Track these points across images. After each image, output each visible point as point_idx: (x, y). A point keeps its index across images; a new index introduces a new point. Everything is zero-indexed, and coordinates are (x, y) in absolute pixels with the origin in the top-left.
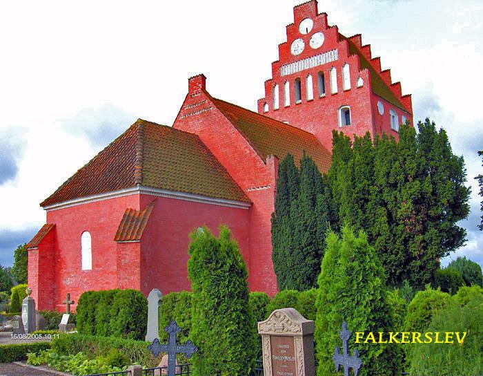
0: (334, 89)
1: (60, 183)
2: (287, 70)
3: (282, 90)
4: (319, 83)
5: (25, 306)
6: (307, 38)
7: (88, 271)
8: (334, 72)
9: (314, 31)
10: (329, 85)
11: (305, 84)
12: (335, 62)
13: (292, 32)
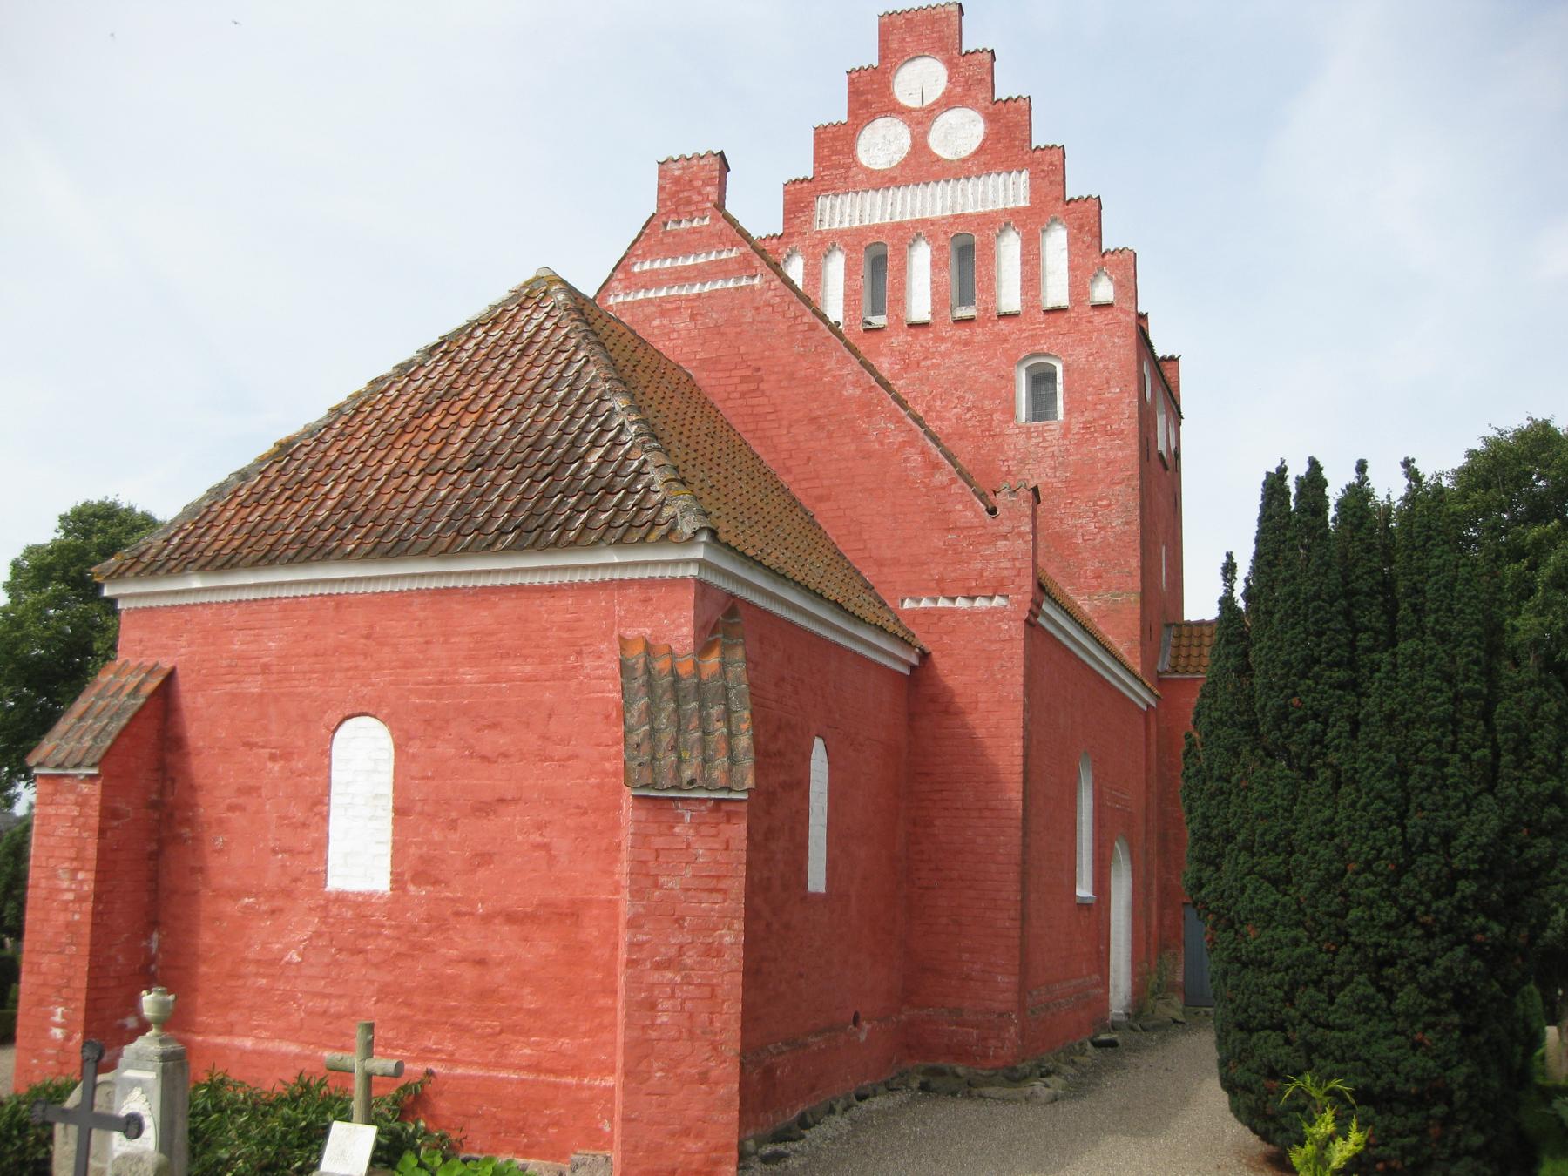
0: (1010, 298)
1: (219, 474)
2: (840, 212)
3: (719, 270)
4: (864, 283)
5: (138, 1083)
6: (920, 120)
7: (359, 904)
8: (1010, 248)
9: (947, 102)
10: (902, 287)
11: (903, 269)
12: (1016, 212)
13: (869, 94)
